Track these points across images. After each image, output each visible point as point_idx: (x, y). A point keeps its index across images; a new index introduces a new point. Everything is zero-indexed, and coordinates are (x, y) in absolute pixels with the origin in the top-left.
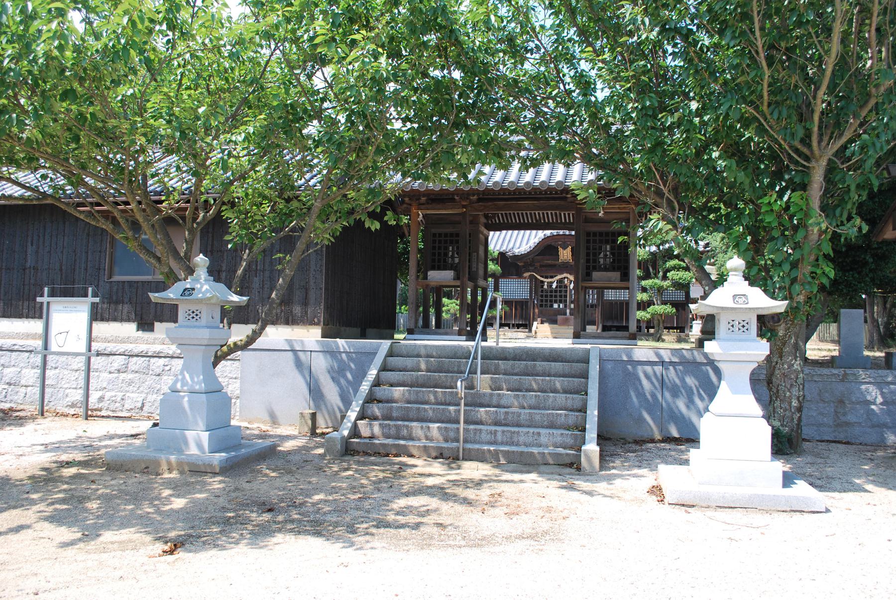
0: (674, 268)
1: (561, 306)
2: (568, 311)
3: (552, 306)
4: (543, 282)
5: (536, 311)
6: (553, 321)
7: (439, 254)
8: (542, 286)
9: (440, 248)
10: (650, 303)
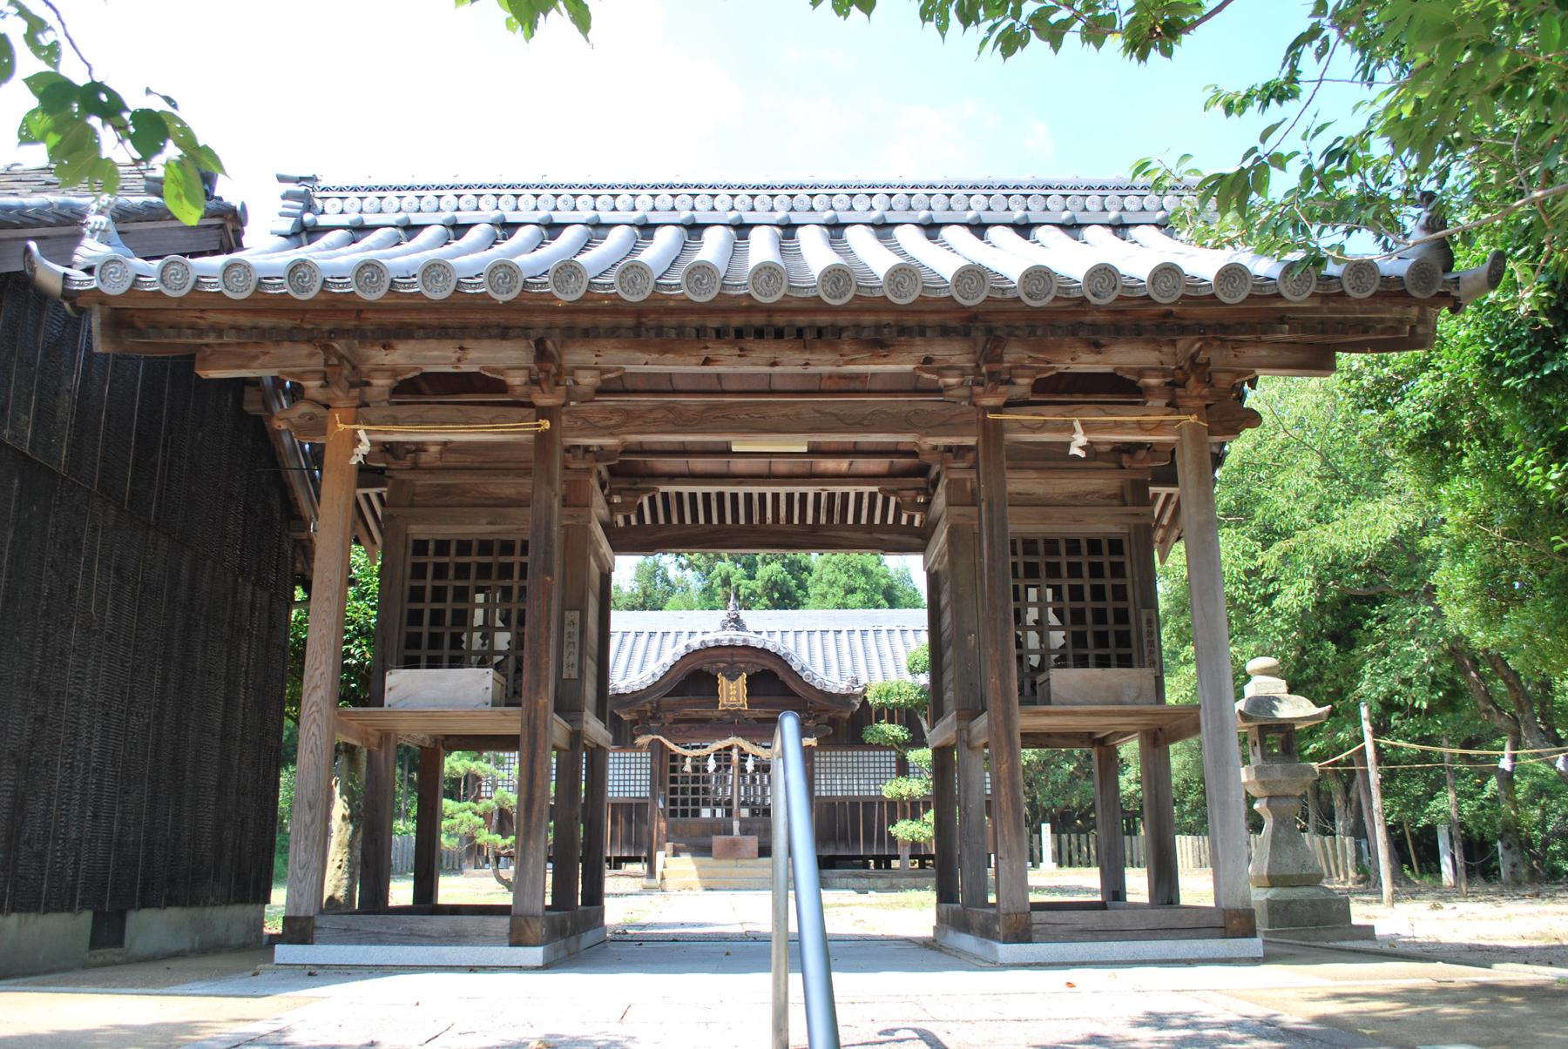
1: (719, 813)
2: (736, 825)
3: (696, 813)
6: (702, 850)
7: (437, 617)
9: (439, 594)
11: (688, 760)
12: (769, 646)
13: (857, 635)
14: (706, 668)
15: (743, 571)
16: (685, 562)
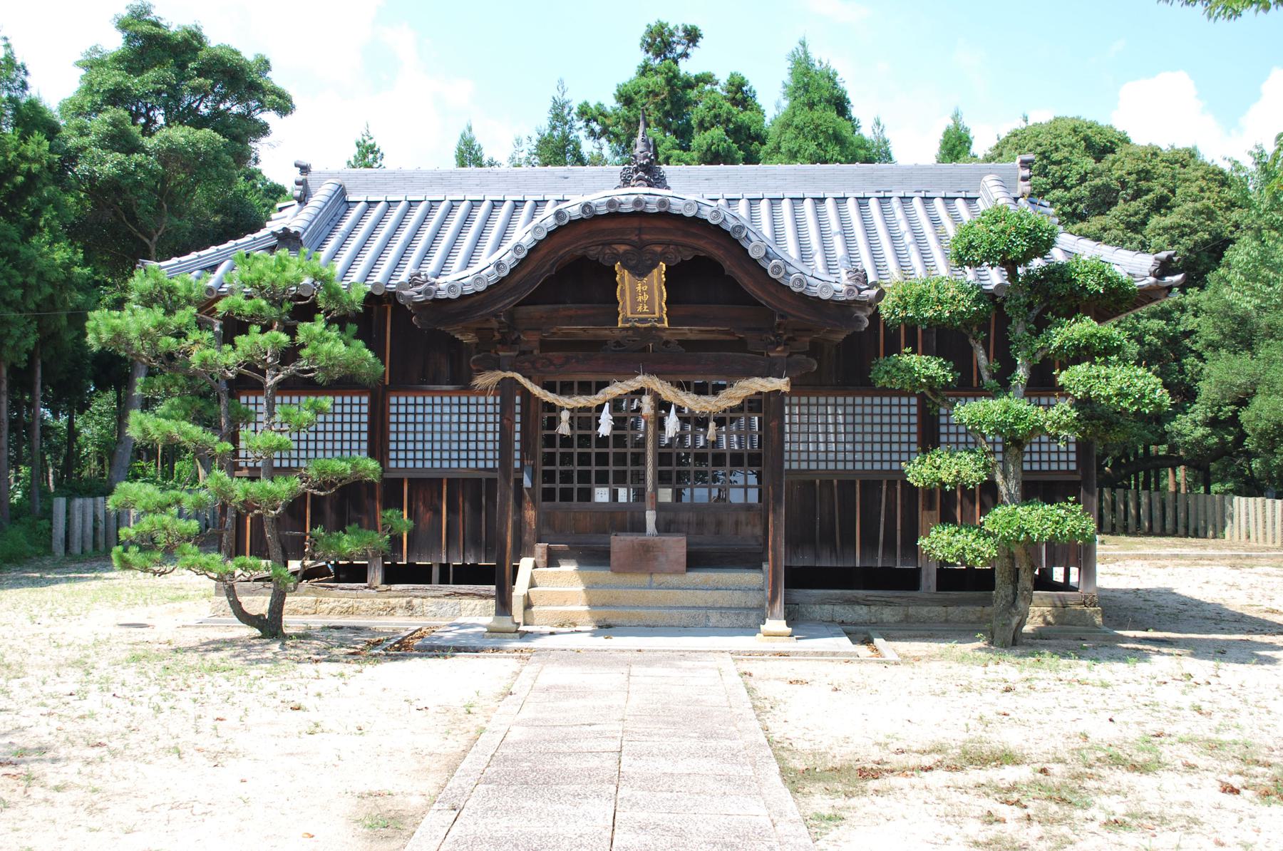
0: (1083, 352)
2: (651, 517)
3: (587, 495)
4: (551, 407)
5: (530, 514)
6: (592, 555)
8: (553, 423)
10: (988, 494)
11: (565, 416)
12: (706, 214)
13: (851, 205)
14: (593, 252)
15: (671, 138)
16: (597, 128)
